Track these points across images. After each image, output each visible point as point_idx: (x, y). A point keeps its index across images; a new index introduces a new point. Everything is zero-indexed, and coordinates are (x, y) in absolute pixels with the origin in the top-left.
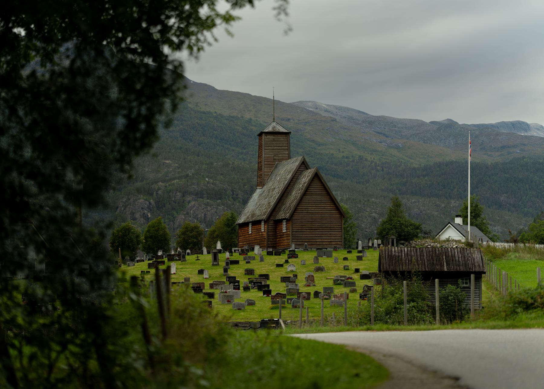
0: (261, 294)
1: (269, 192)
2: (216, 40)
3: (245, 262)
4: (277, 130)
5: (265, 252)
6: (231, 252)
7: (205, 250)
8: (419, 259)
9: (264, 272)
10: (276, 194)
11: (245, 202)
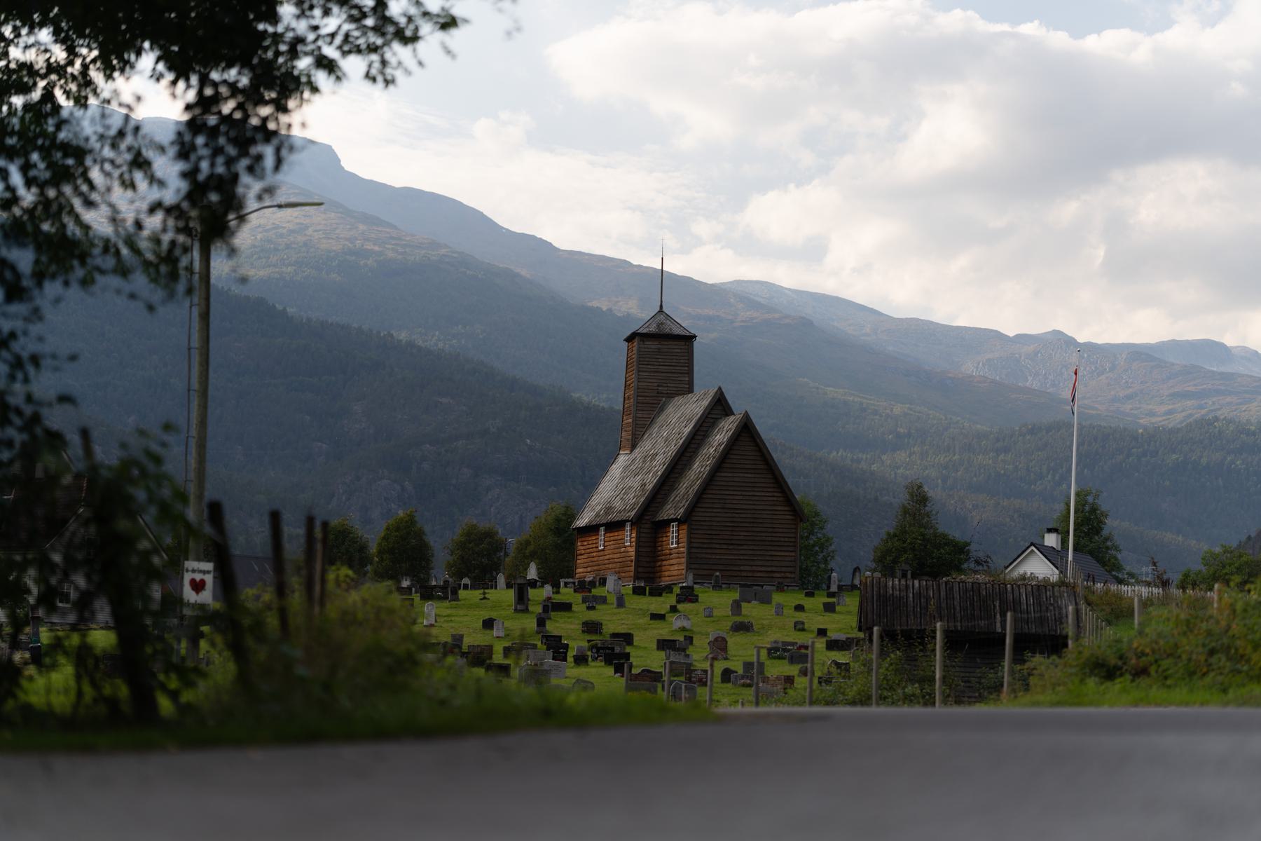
0: (610, 671)
1: (644, 462)
2: (420, 64)
3: (584, 606)
4: (667, 331)
5: (628, 589)
6: (556, 586)
7: (501, 579)
8: (944, 605)
9: (622, 629)
10: (659, 466)
11: (591, 485)
